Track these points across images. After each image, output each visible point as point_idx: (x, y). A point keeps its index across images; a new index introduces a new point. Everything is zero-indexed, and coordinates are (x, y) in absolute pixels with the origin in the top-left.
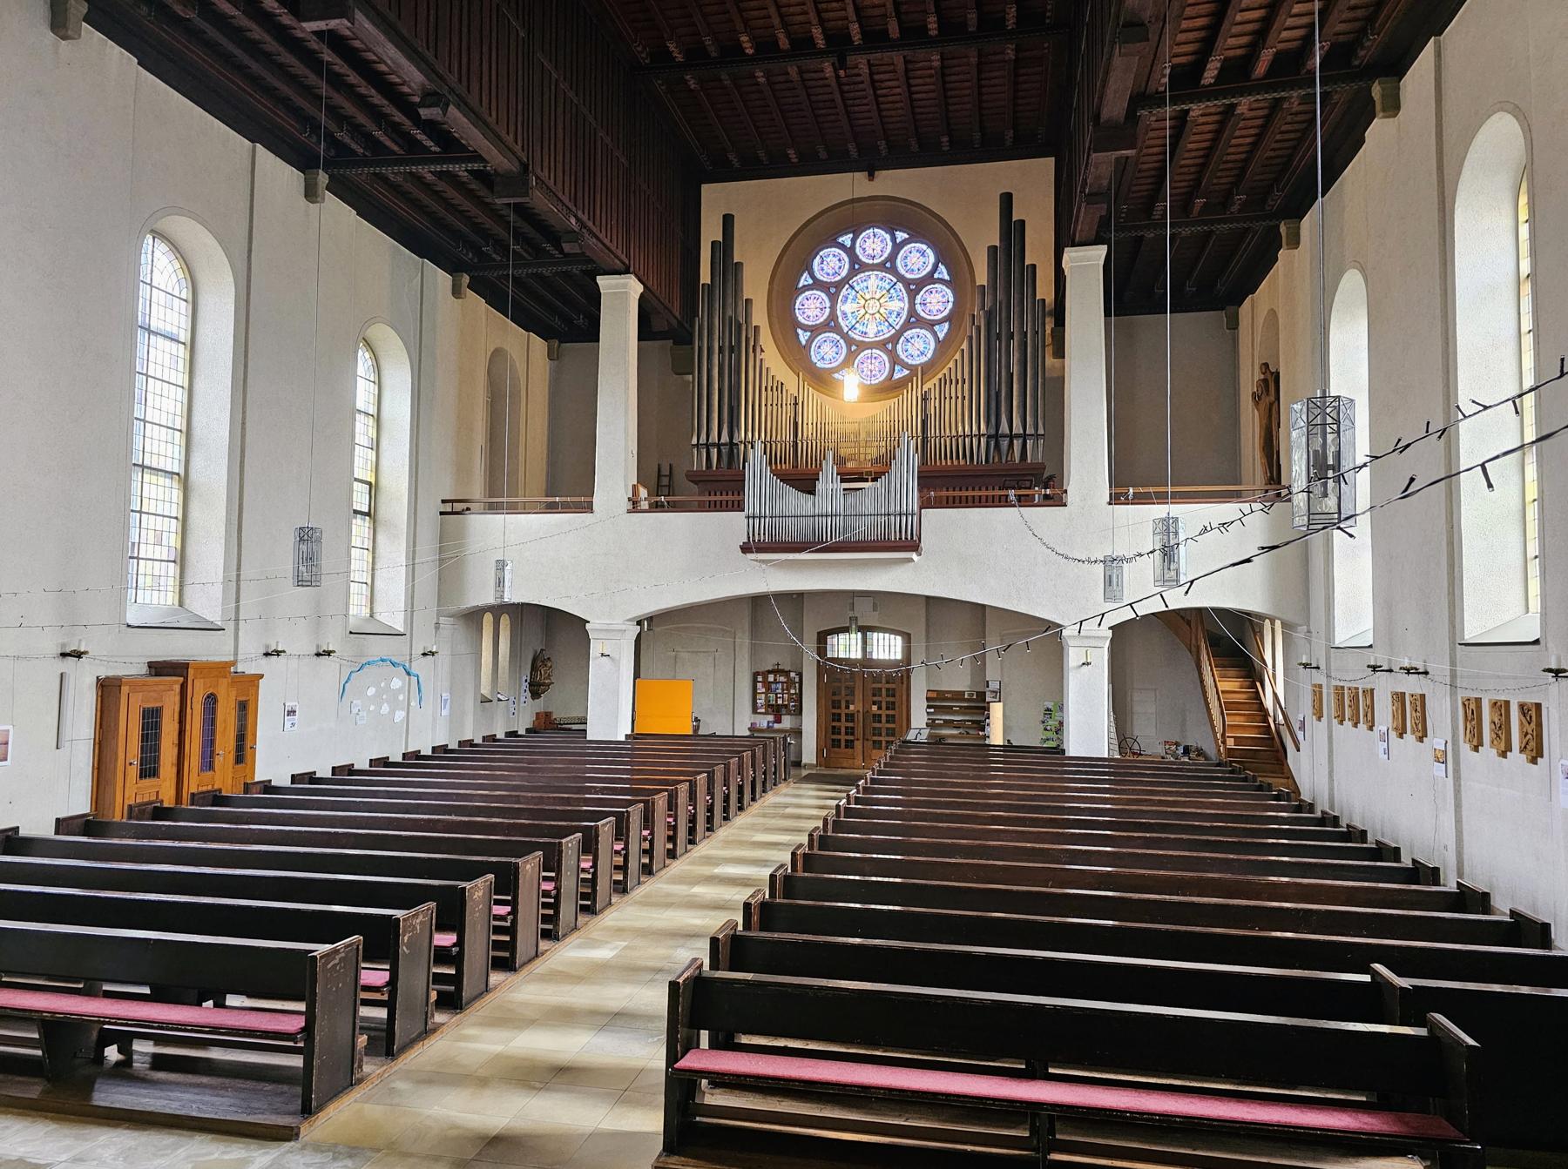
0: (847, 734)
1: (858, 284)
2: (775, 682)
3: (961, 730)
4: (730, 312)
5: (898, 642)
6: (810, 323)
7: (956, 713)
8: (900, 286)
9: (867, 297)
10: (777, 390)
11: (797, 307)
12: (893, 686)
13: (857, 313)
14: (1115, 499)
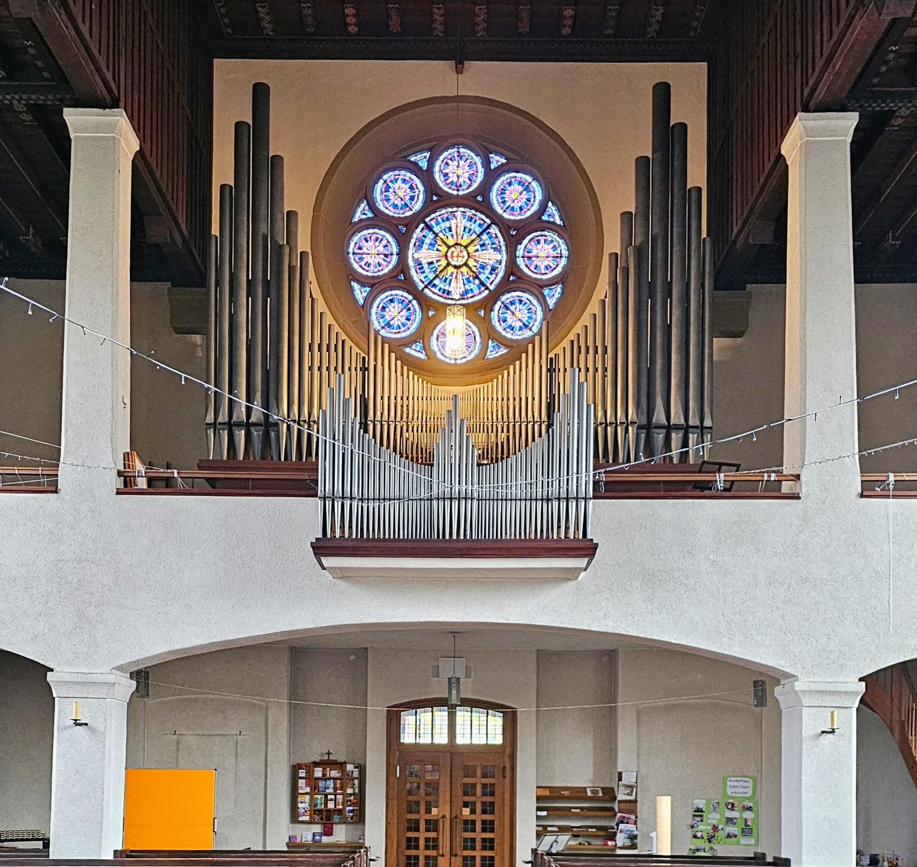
0: (427, 848)
1: (438, 224)
2: (324, 778)
3: (580, 840)
4: (264, 228)
5: (496, 721)
6: (370, 274)
7: (577, 816)
8: (494, 230)
9: (451, 242)
10: (336, 350)
11: (351, 250)
12: (492, 781)
13: (436, 265)
14: (868, 490)
